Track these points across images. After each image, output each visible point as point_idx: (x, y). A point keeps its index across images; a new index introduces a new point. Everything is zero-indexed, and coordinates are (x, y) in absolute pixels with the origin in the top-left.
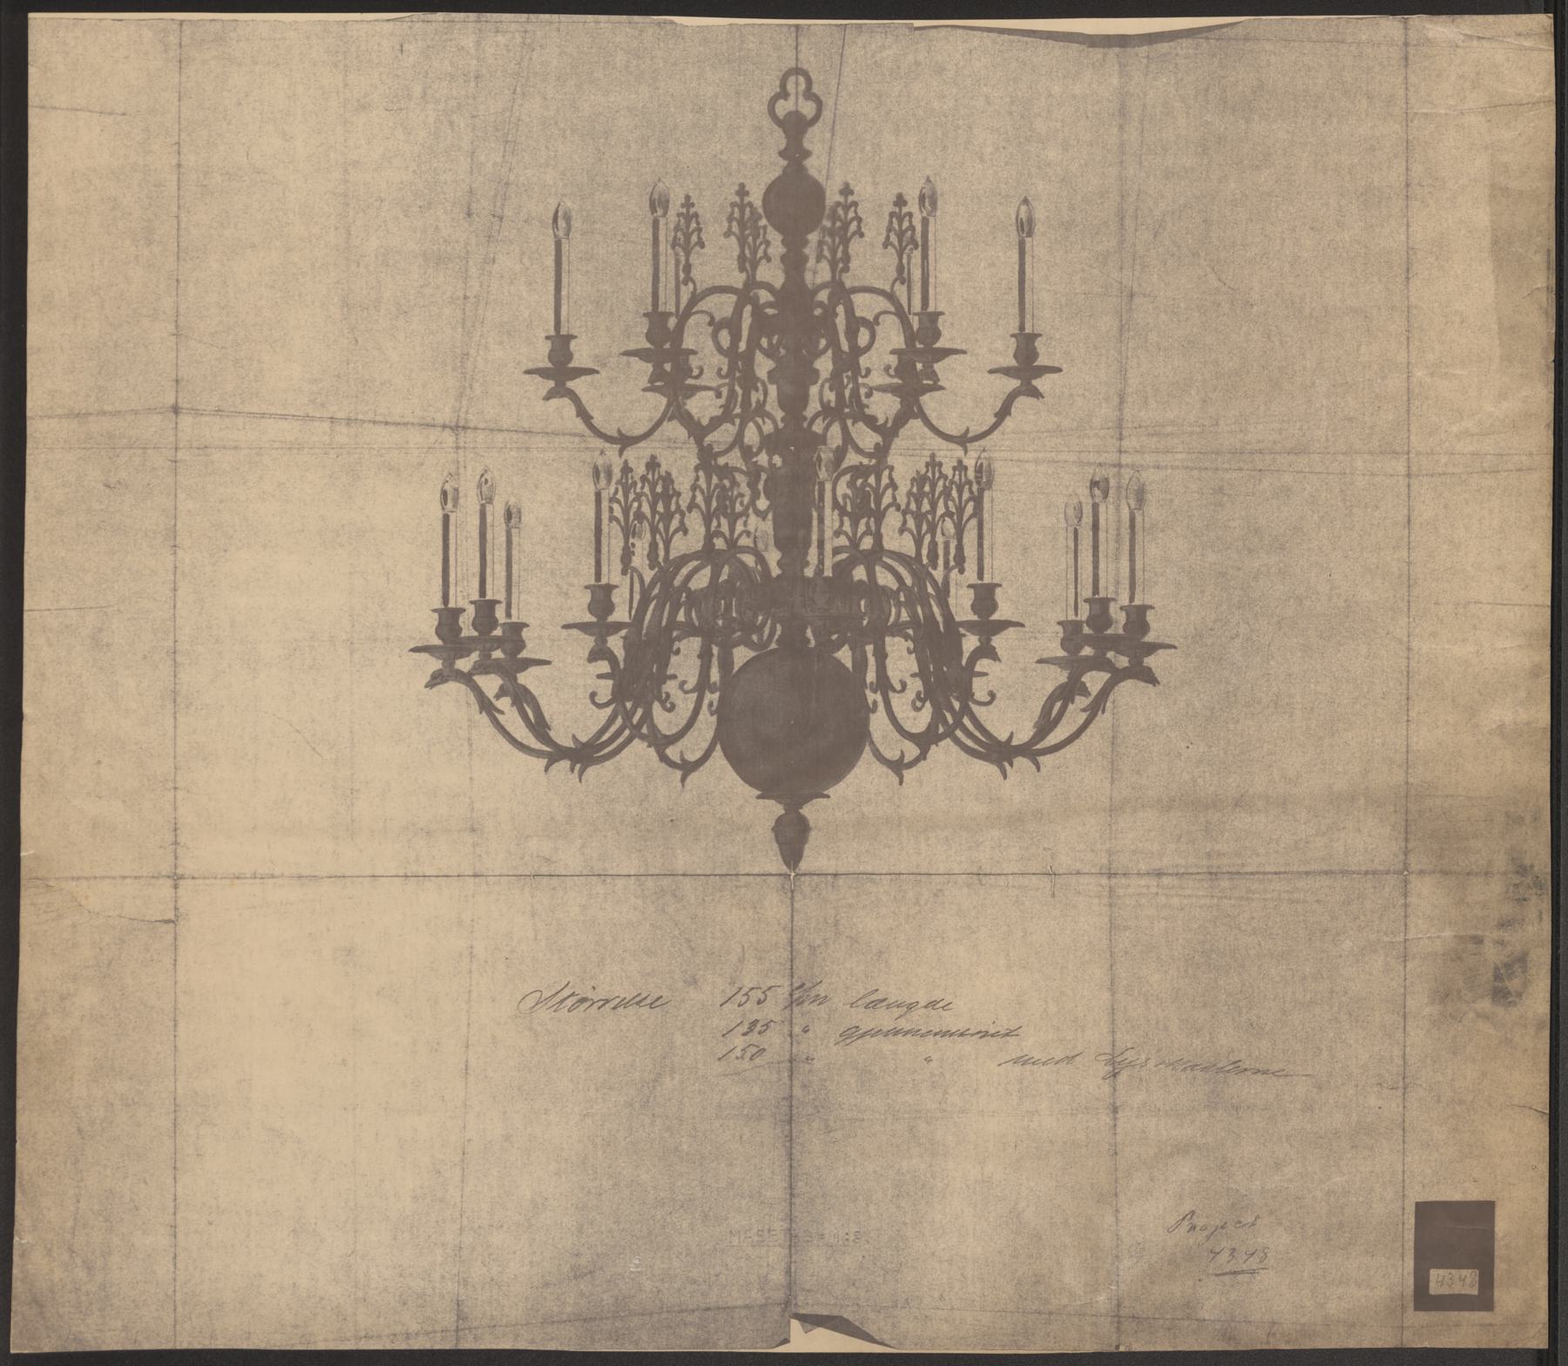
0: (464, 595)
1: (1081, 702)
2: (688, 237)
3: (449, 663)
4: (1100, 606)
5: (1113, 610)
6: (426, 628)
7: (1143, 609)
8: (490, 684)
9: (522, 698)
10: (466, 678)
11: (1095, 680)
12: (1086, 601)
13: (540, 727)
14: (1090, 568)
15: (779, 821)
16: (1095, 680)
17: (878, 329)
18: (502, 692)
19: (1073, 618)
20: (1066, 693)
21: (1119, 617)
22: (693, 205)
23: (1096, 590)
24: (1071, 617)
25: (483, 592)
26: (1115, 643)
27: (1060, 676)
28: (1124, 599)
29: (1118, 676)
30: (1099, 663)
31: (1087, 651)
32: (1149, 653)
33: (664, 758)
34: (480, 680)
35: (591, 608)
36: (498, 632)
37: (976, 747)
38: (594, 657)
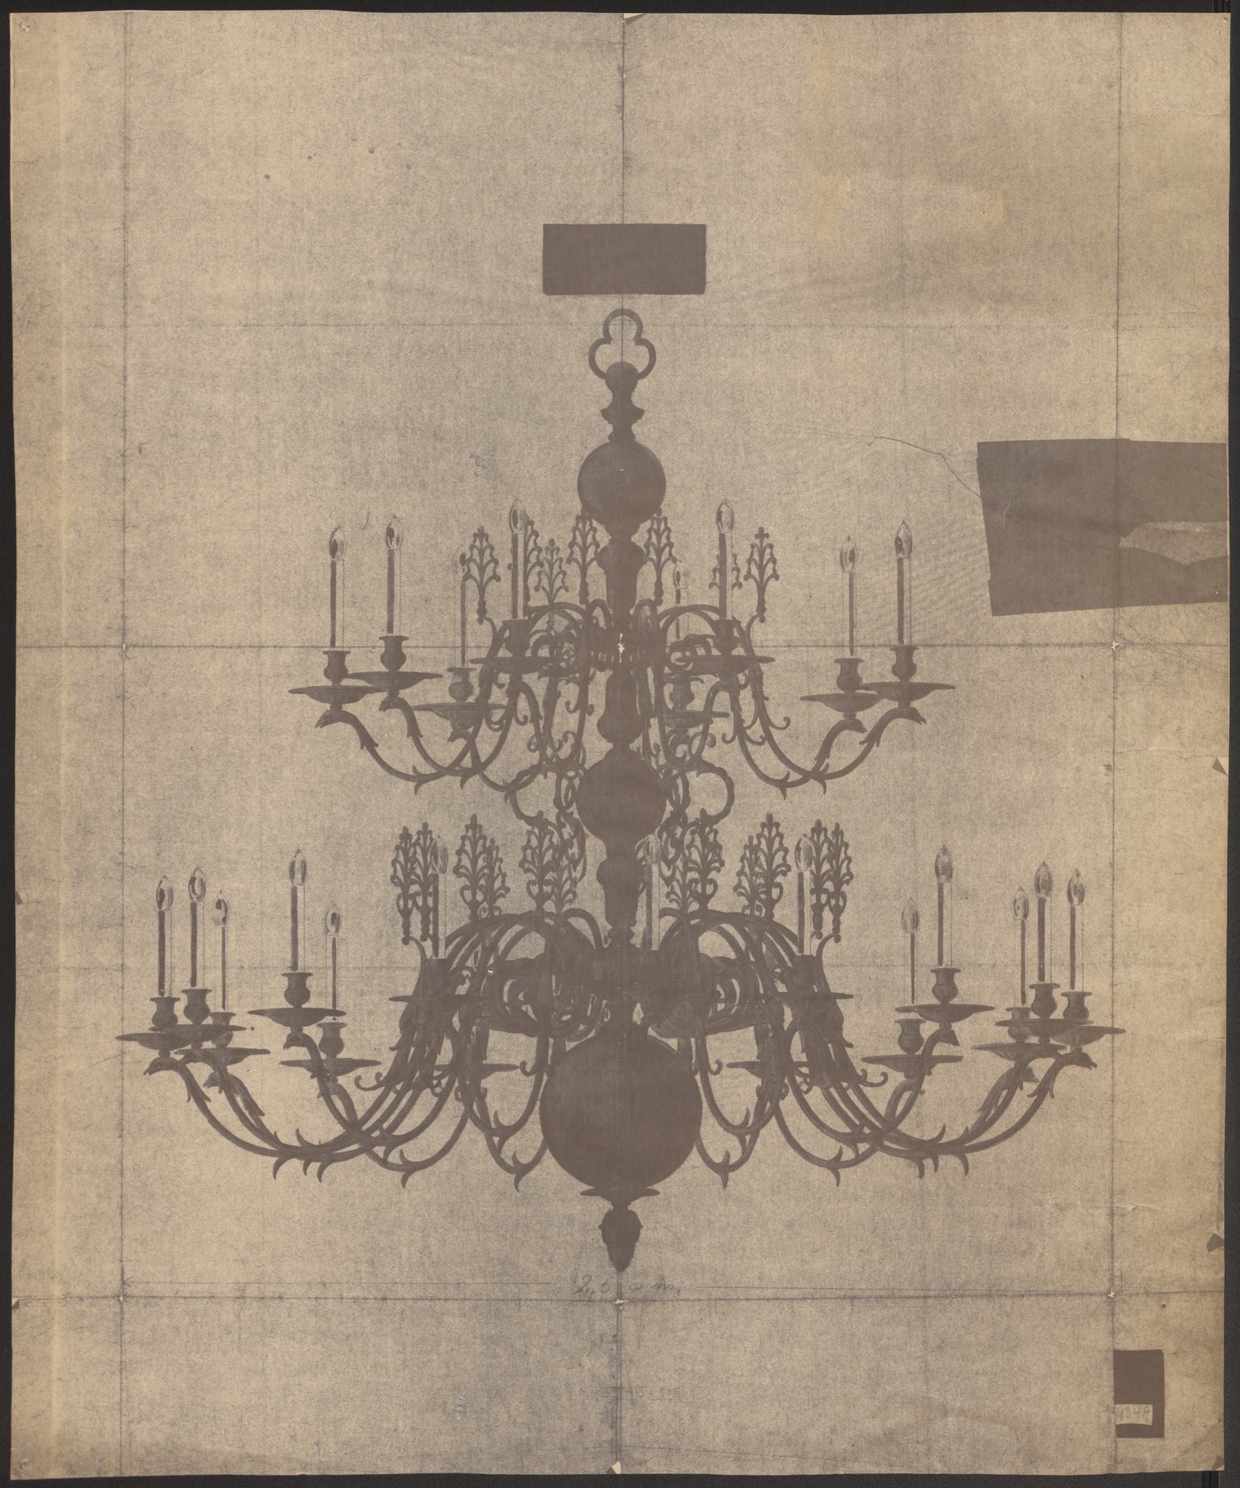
0: (179, 982)
1: (1029, 1087)
2: (762, 569)
3: (165, 1053)
4: (1045, 993)
5: (1056, 994)
6: (143, 1018)
7: (1082, 996)
8: (202, 1071)
9: (231, 1087)
10: (180, 1068)
11: (1040, 1066)
12: (1032, 987)
13: (251, 1113)
14: (1036, 960)
15: (608, 1216)
16: (1040, 1066)
17: (499, 795)
18: (211, 1082)
19: (221, 1010)
20: (1012, 1082)
21: (1062, 1004)
22: (767, 536)
23: (1041, 976)
24: (1020, 1005)
25: (193, 981)
26: (1057, 1028)
27: (1005, 1065)
28: (1066, 988)
29: (1062, 1062)
30: (1046, 1050)
31: (1034, 1040)
32: (1089, 1040)
33: (496, 1151)
34: (191, 1066)
35: (288, 995)
36: (209, 1021)
37: (975, 1141)
38: (291, 1042)
